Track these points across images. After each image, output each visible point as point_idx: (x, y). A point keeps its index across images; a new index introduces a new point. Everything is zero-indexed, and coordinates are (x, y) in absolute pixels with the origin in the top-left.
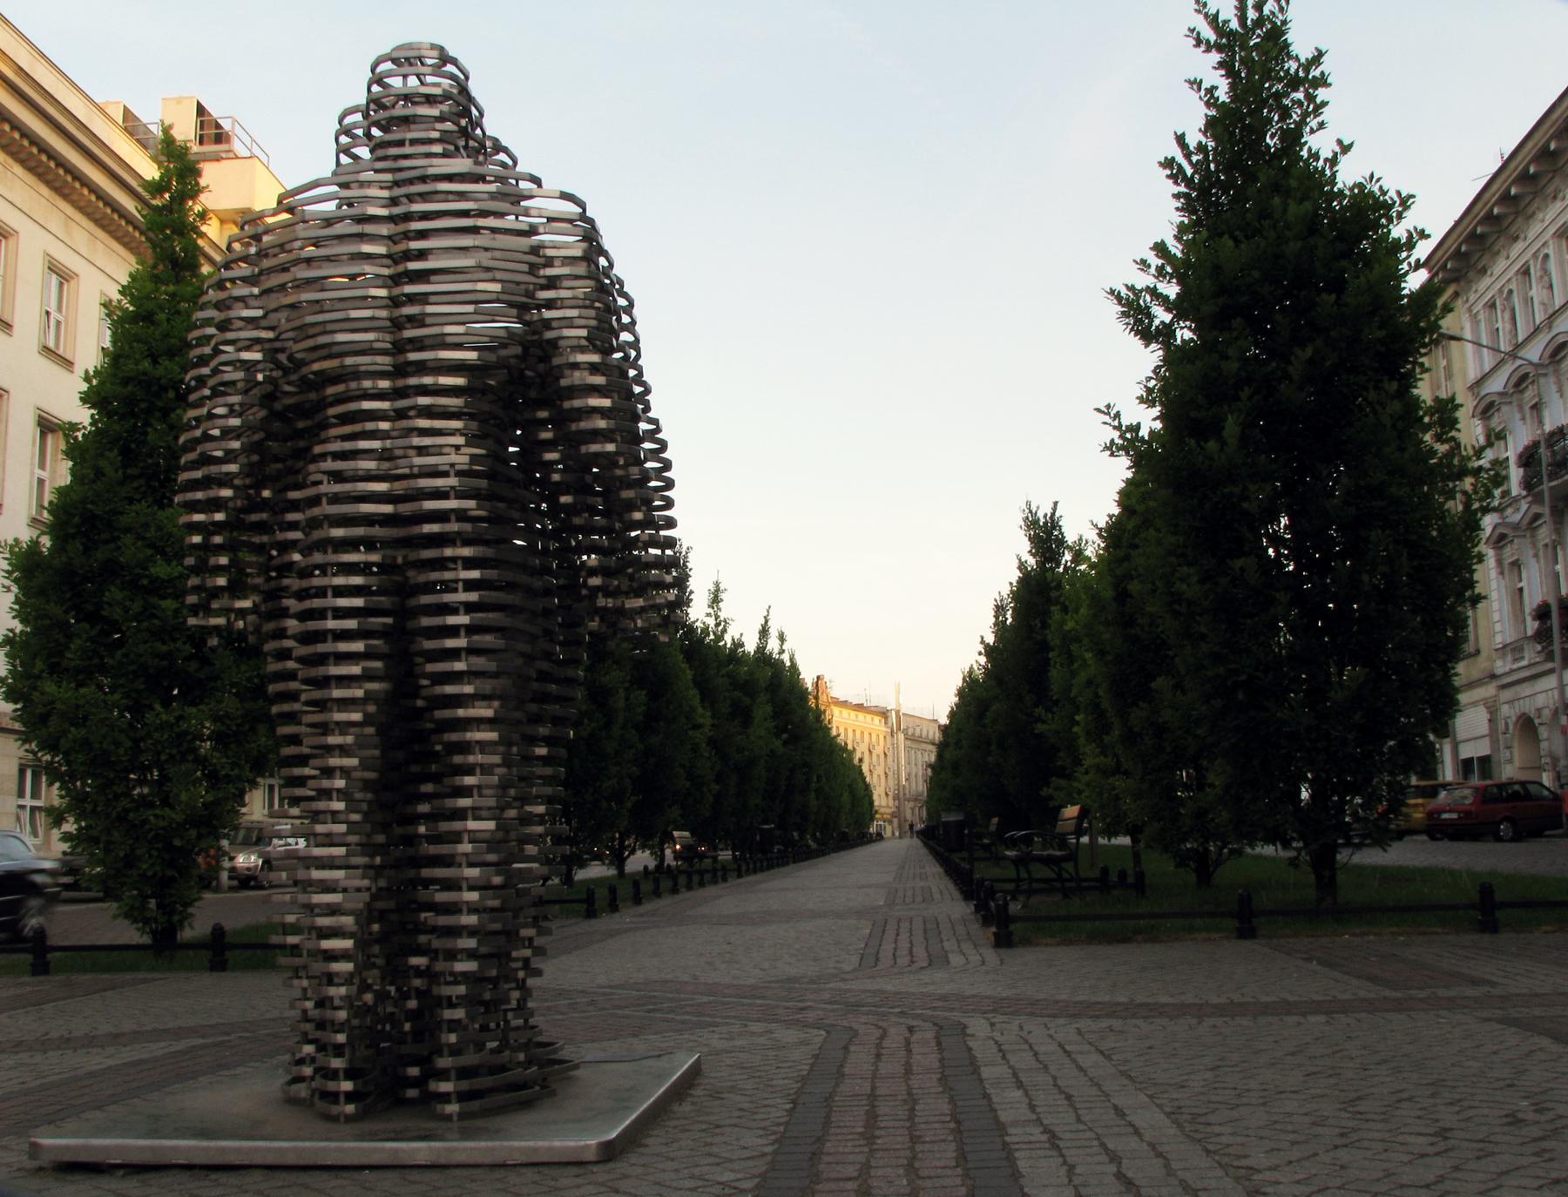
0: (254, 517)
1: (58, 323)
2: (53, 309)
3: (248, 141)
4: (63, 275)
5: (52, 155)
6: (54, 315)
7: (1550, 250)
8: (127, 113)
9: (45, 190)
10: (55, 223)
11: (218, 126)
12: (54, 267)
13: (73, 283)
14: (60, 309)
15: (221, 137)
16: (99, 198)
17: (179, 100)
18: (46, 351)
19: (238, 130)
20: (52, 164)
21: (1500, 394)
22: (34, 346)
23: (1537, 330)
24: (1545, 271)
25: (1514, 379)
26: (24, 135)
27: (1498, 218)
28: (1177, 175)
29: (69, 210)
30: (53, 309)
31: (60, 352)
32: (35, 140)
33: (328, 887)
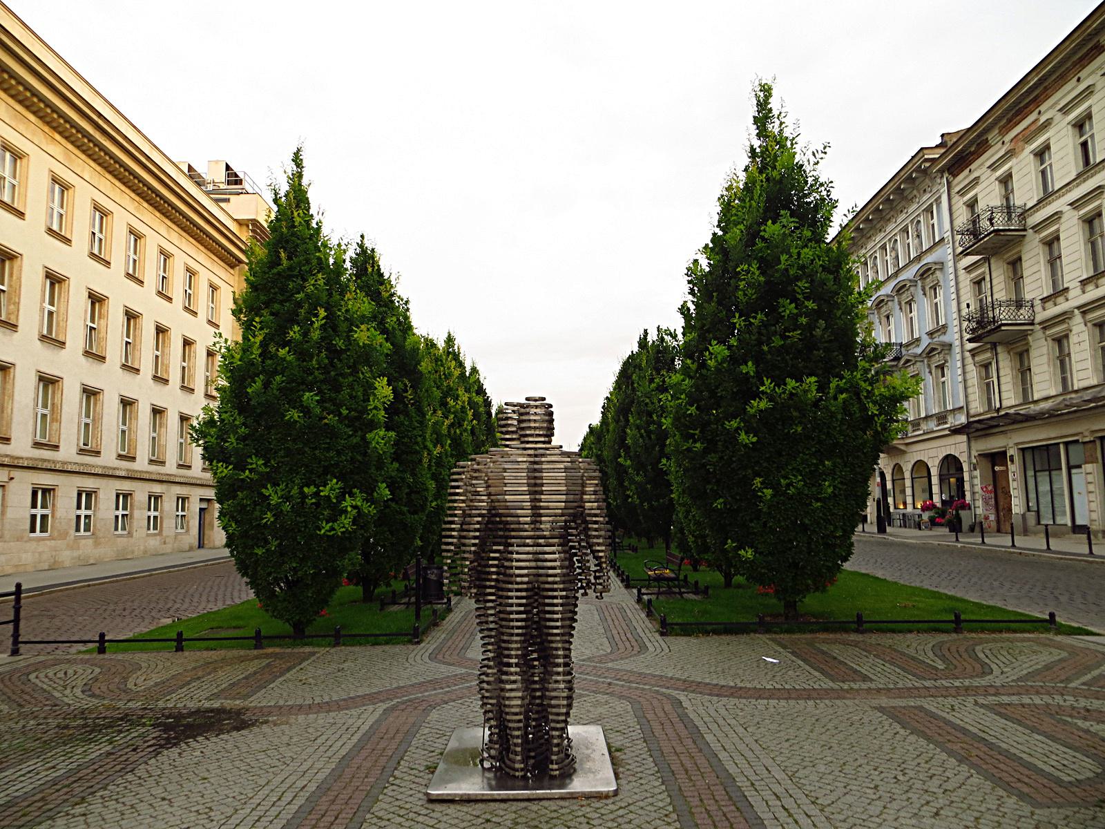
0: (1061, 800)
1: (101, 240)
2: (97, 231)
3: (252, 183)
4: (137, 236)
5: (162, 197)
6: (98, 235)
7: (921, 219)
8: (190, 168)
9: (158, 214)
10: (163, 230)
11: (236, 176)
12: (97, 207)
13: (71, 191)
14: (101, 232)
15: (238, 182)
16: (149, 189)
17: (217, 162)
18: (93, 256)
19: (247, 178)
20: (112, 162)
21: (888, 296)
22: (181, 307)
23: (911, 262)
24: (875, 265)
25: (921, 271)
26: (149, 188)
27: (914, 179)
28: (643, 343)
29: (169, 223)
30: (97, 231)
31: (15, 206)
32: (150, 188)
33: (596, 522)
